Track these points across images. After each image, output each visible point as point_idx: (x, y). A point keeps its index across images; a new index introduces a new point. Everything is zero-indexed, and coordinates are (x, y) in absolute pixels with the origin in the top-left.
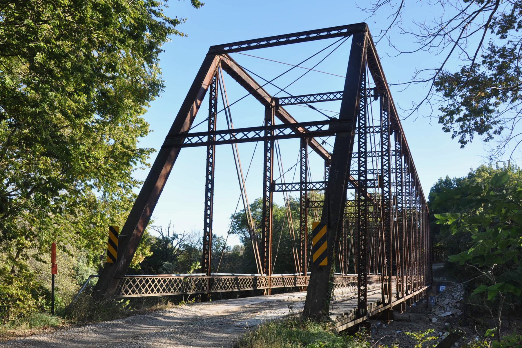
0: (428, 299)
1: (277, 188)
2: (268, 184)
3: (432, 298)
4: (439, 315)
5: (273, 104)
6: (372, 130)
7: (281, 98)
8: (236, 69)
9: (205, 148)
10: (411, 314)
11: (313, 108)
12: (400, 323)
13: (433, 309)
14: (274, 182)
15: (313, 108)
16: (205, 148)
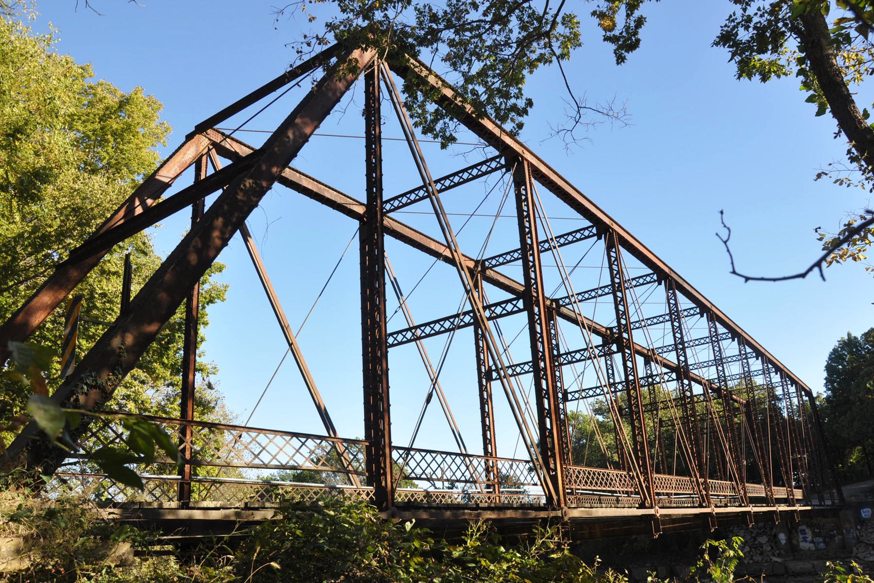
0: (842, 534)
1: (570, 397)
2: (560, 395)
3: (848, 532)
4: (866, 559)
5: (554, 306)
6: (510, 372)
7: (561, 299)
8: (502, 280)
9: (472, 327)
10: (815, 562)
11: (428, 400)
12: (799, 578)
13: (855, 549)
14: (566, 390)
15: (428, 400)
16: (472, 327)
